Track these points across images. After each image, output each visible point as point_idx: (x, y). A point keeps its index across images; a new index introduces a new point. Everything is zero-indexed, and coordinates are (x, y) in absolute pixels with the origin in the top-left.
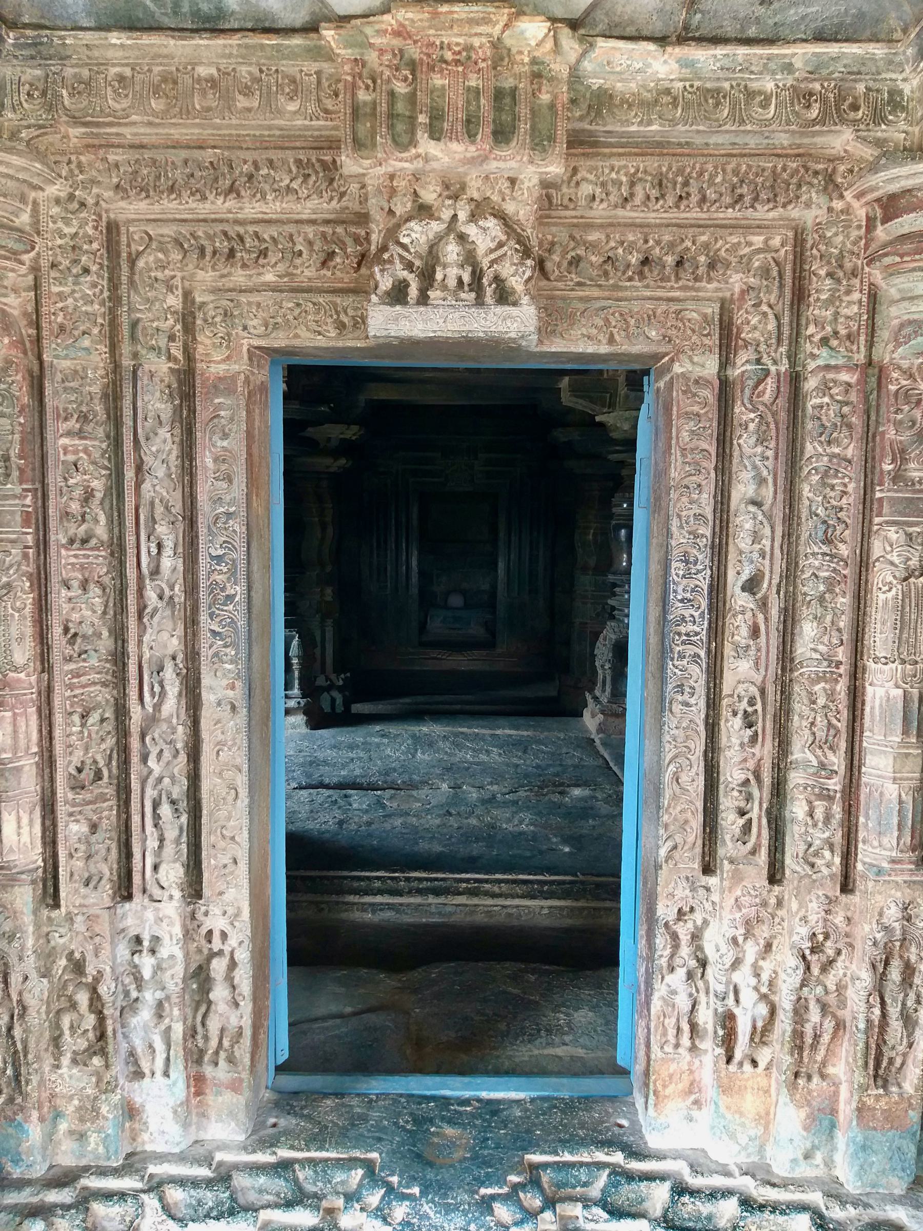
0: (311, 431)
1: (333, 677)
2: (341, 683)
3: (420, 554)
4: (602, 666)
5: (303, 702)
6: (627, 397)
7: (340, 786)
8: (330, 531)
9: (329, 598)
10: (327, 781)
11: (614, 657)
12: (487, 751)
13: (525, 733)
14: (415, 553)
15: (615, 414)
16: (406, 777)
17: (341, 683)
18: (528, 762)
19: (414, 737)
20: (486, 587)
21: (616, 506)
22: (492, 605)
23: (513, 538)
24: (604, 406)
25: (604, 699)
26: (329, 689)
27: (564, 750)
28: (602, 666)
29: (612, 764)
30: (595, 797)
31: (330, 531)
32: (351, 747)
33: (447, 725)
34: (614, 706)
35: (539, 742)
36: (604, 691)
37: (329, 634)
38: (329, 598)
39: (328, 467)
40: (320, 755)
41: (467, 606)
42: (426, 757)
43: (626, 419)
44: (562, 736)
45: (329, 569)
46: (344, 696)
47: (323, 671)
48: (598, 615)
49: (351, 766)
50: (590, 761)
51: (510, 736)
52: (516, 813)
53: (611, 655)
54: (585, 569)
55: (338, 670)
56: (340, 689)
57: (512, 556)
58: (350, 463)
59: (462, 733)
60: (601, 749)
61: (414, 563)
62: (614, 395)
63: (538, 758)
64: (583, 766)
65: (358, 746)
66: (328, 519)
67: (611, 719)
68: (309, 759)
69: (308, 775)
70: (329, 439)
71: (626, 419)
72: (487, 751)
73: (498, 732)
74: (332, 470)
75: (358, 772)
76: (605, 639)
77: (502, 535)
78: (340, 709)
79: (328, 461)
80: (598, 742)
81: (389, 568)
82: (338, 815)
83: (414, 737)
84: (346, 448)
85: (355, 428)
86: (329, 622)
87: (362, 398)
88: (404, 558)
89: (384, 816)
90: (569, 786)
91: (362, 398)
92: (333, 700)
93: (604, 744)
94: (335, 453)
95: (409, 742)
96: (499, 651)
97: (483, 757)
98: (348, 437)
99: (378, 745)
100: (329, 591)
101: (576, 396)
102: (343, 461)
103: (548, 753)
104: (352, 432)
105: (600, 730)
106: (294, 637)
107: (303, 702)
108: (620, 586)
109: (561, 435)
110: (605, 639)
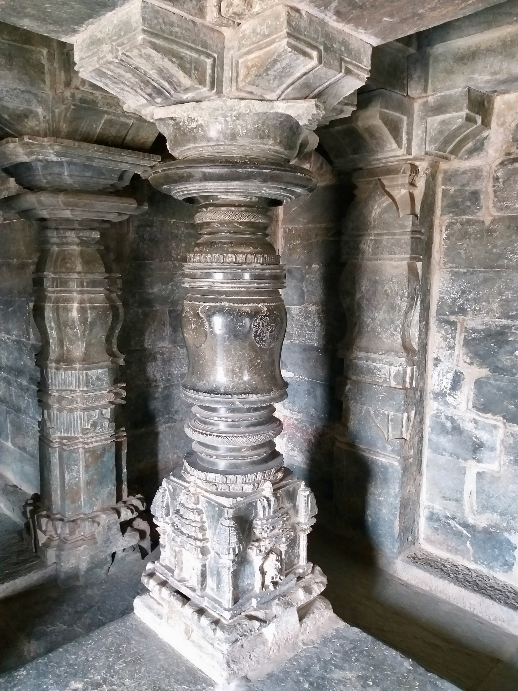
48: (94, 425)
101: (155, 47)
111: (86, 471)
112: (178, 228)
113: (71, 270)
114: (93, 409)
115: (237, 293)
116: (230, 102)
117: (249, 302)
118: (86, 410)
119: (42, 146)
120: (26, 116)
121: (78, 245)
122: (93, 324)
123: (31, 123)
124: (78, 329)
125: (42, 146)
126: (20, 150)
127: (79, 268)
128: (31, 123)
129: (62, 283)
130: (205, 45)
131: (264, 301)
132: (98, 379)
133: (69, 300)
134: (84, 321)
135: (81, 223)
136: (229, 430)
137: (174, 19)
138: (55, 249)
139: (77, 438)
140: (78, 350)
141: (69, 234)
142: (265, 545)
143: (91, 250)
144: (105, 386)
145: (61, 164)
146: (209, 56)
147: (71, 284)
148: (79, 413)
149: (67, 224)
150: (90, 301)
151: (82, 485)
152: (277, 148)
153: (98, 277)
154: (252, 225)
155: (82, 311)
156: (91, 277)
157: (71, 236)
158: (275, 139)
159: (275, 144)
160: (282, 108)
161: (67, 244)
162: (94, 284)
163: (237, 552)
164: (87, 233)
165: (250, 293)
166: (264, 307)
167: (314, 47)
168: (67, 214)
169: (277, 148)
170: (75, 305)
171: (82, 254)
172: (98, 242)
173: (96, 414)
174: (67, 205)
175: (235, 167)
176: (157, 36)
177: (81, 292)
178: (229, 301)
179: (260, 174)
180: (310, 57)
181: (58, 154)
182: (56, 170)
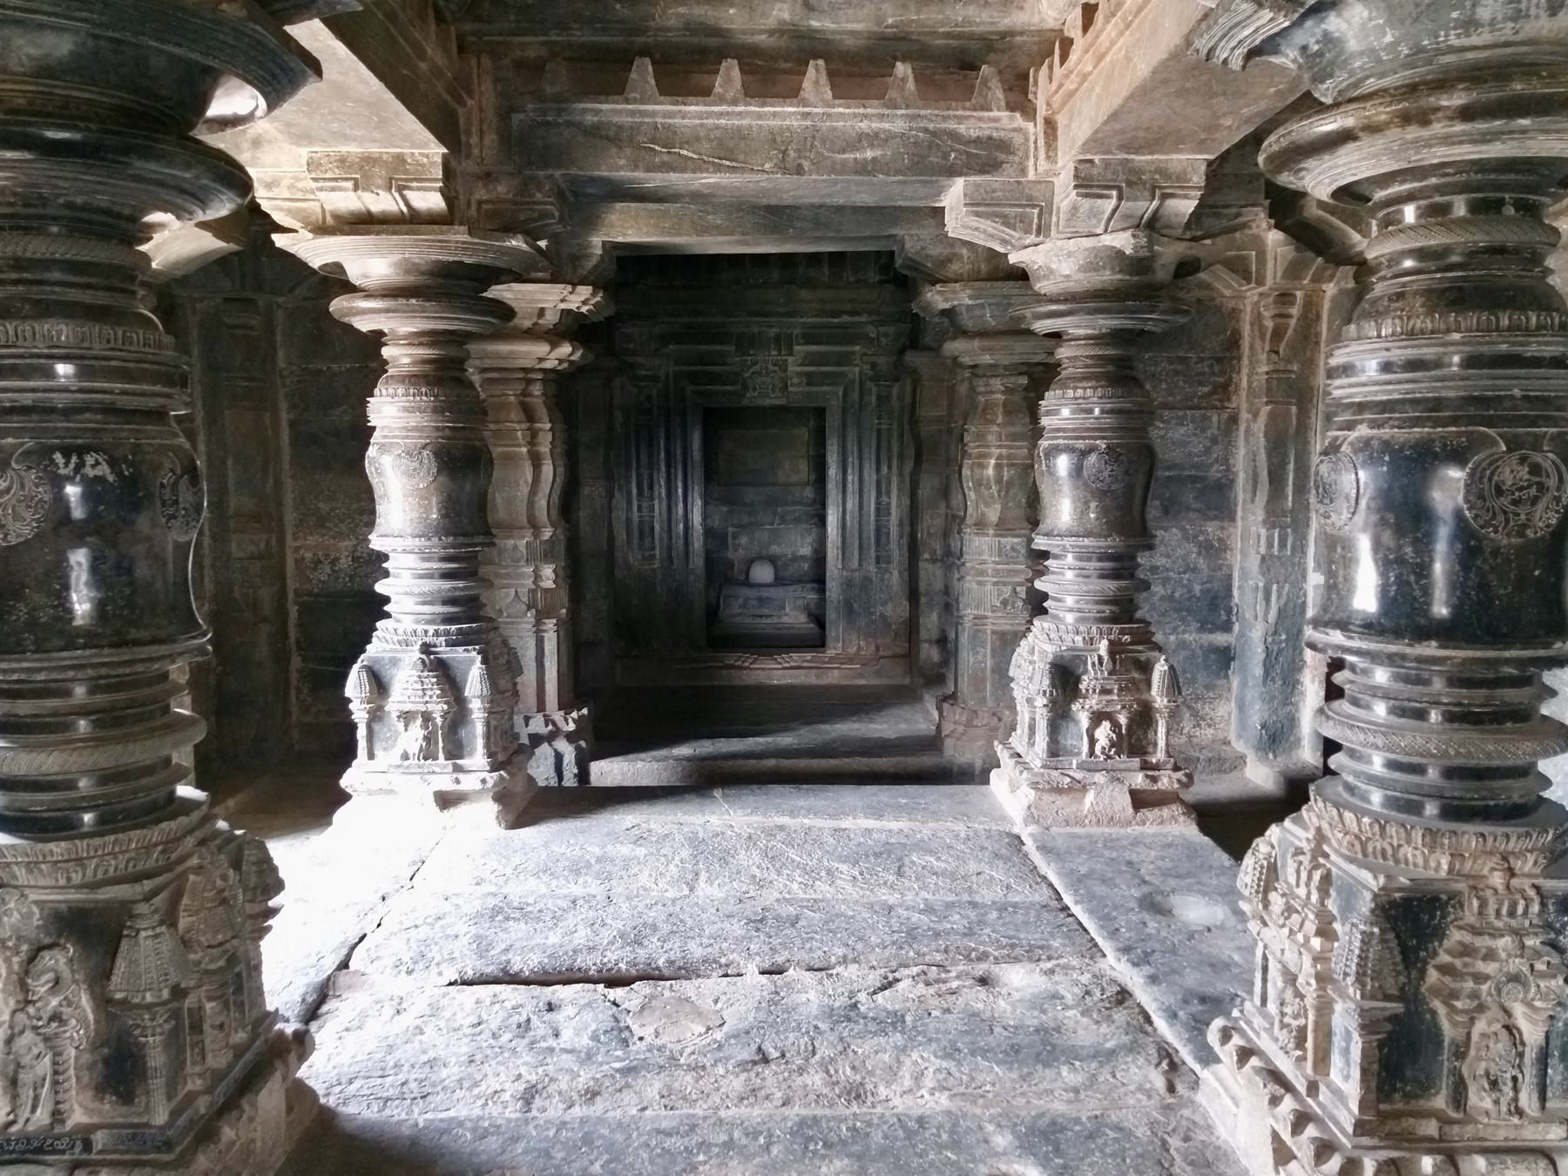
0: (498, 292)
1: (558, 716)
2: (572, 727)
3: (705, 504)
4: (1029, 701)
5: (492, 778)
6: (1075, 209)
7: (544, 979)
8: (548, 469)
9: (549, 584)
10: (516, 965)
11: (1053, 685)
12: (829, 872)
13: (894, 825)
14: (699, 503)
15: (1048, 245)
16: (675, 945)
17: (572, 727)
18: (909, 897)
19: (695, 842)
20: (806, 550)
21: (1048, 413)
22: (819, 580)
23: (850, 478)
24: (1027, 232)
25: (1036, 764)
26: (550, 738)
27: (973, 867)
28: (1029, 701)
29: (1068, 900)
30: (1056, 996)
31: (548, 469)
32: (576, 870)
33: (755, 811)
34: (1055, 773)
35: (924, 847)
36: (1031, 743)
37: (551, 644)
38: (549, 584)
39: (541, 360)
40: (517, 891)
41: (779, 581)
42: (717, 893)
43: (1069, 255)
44: (961, 828)
45: (547, 533)
46: (578, 749)
47: (541, 707)
48: (1005, 603)
49: (571, 920)
50: (1025, 894)
51: (868, 831)
52: (904, 1050)
53: (1047, 682)
54: (981, 525)
55: (565, 706)
56: (571, 737)
57: (849, 505)
58: (579, 353)
59: (781, 828)
60: (1037, 858)
61: (696, 518)
62: (1046, 210)
63: (924, 887)
64: (1015, 906)
65: (589, 865)
66: (545, 448)
67: (1048, 798)
68: (491, 902)
69: (482, 953)
70: (542, 312)
71: (1069, 255)
72: (829, 872)
73: (846, 823)
74: (548, 365)
75: (581, 937)
76: (1032, 652)
77: (833, 471)
78: (570, 781)
79: (541, 349)
80: (1030, 846)
81: (657, 527)
82: (526, 1068)
83: (695, 842)
84: (573, 328)
85: (585, 291)
86: (550, 624)
87: (597, 241)
88: (681, 511)
89: (626, 1072)
90: (997, 961)
91: (597, 241)
92: (559, 758)
93: (1043, 848)
94: (554, 336)
95: (685, 853)
96: (830, 652)
97: (823, 888)
98: (573, 307)
99: (627, 863)
100: (548, 571)
101: (977, 214)
102: (565, 349)
103: (944, 873)
104: (580, 299)
105: (1031, 818)
106: (472, 661)
107: (492, 778)
108: (1056, 557)
109: (936, 298)
110: (1032, 652)
111: (993, 657)
112: (1156, 364)
113: (993, 422)
114: (1004, 584)
115: (1074, 430)
116: (1059, 243)
117: (1084, 438)
118: (995, 584)
119: (954, 292)
120: (950, 261)
121: (1003, 392)
122: (1010, 483)
123: (955, 267)
124: (994, 489)
125: (954, 292)
126: (938, 298)
127: (1000, 420)
128: (955, 267)
129: (980, 437)
130: (1030, 198)
131: (1103, 438)
132: (1013, 549)
133: (986, 456)
134: (999, 480)
135: (1006, 368)
136: (1394, 720)
137: (997, 186)
138: (982, 399)
139: (986, 617)
140: (993, 514)
141: (992, 381)
142: (1094, 702)
143: (1017, 398)
144: (1022, 559)
145: (982, 306)
146: (1034, 206)
147: (990, 437)
148: (989, 587)
149: (993, 370)
150: (1009, 457)
151: (988, 672)
152: (1119, 276)
153: (1018, 429)
154: (1099, 357)
155: (998, 467)
156: (1013, 429)
157: (997, 384)
158: (1112, 269)
159: (1114, 273)
160: (1108, 240)
161: (992, 392)
162: (1014, 437)
163: (350, 184)
164: (1013, 379)
165: (1087, 430)
166: (1102, 444)
167: (1111, 188)
168: (987, 359)
169: (1119, 276)
170: (993, 461)
171: (1005, 404)
172: (1026, 389)
173: (1007, 591)
174: (984, 350)
175: (1078, 301)
176: (978, 205)
177: (999, 447)
178: (1065, 438)
179: (1081, 310)
180: (1109, 197)
181: (970, 297)
182: (978, 312)
